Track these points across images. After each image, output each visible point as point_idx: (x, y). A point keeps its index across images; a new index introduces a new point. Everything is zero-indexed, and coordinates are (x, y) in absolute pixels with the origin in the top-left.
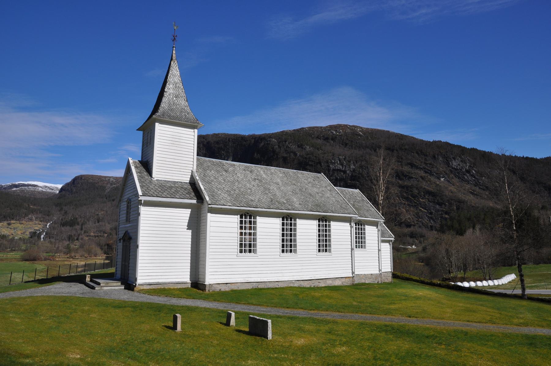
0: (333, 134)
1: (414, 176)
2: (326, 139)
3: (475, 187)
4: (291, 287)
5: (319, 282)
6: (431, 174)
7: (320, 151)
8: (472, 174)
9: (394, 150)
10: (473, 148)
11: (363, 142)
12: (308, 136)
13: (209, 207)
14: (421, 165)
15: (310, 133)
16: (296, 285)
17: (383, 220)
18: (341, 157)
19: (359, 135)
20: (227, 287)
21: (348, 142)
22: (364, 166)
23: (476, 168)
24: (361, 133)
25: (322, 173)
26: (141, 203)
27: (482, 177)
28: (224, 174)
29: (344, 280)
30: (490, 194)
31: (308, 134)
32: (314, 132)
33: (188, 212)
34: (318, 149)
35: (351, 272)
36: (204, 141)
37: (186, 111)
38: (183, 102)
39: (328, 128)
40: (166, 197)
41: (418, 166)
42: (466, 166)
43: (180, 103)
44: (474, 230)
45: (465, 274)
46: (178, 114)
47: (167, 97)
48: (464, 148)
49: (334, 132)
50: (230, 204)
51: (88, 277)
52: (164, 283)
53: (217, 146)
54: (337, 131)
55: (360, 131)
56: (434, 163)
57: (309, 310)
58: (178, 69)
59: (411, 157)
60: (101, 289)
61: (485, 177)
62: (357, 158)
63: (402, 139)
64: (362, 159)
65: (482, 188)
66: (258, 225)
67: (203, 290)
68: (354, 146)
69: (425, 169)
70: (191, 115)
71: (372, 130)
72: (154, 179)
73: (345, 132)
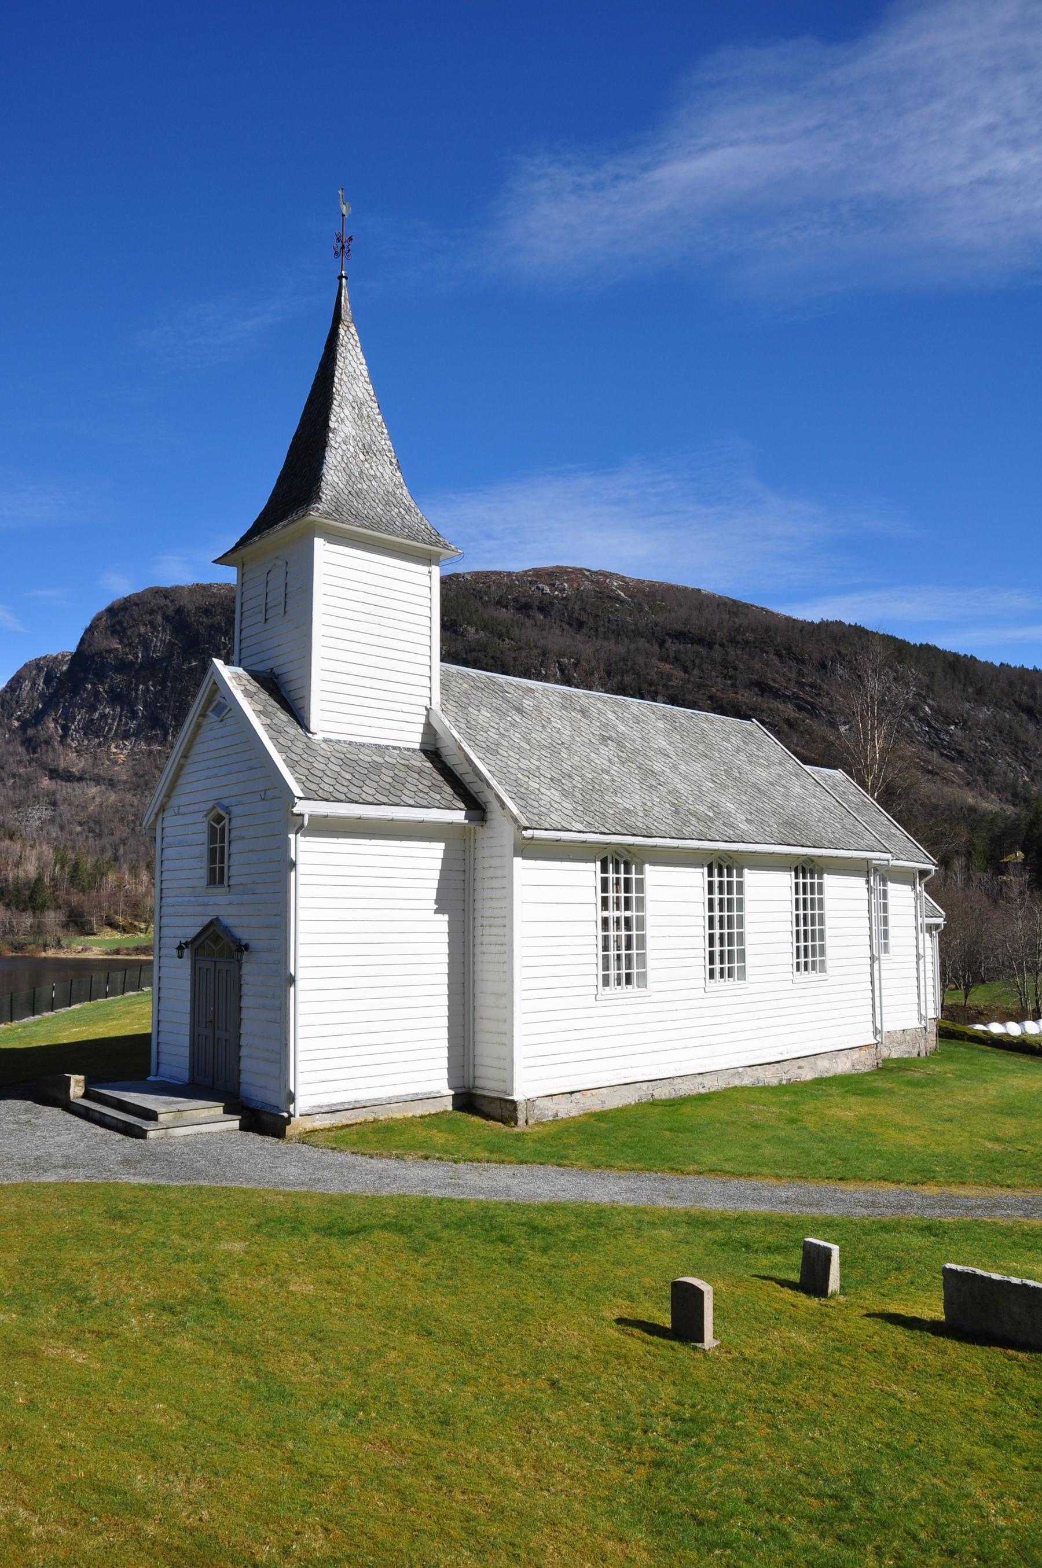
0: (543, 594)
1: (767, 718)
2: (524, 608)
3: (930, 753)
4: (735, 1088)
5: (800, 1068)
6: (813, 711)
7: (507, 641)
8: (922, 714)
9: (715, 644)
10: (927, 645)
11: (628, 619)
12: (472, 597)
13: (524, 838)
14: (786, 688)
15: (478, 589)
16: (747, 1081)
17: (934, 864)
18: (566, 661)
19: (618, 599)
20: (573, 1105)
21: (584, 617)
22: (631, 689)
23: (933, 700)
24: (623, 594)
25: (754, 720)
26: (302, 826)
27: (949, 725)
28: (518, 720)
29: (855, 1055)
30: (967, 770)
31: (471, 591)
32: (489, 587)
33: (435, 851)
34: (500, 637)
35: (872, 1029)
36: (166, 606)
37: (400, 504)
38: (388, 472)
39: (529, 576)
40: (375, 802)
41: (779, 690)
42: (907, 693)
43: (378, 474)
44: (949, 873)
45: (966, 997)
46: (378, 509)
47: (340, 450)
48: (904, 643)
49: (547, 590)
50: (581, 827)
51: (77, 1081)
52: (376, 1103)
53: (205, 620)
54: (553, 585)
55: (620, 588)
56: (822, 684)
57: (908, 1184)
58: (361, 355)
59: (760, 664)
60: (166, 1134)
61: (956, 724)
62: (610, 665)
63: (736, 614)
64: (624, 667)
65: (947, 756)
66: (650, 893)
67: (504, 1120)
68: (601, 629)
69: (797, 698)
70: (417, 514)
71: (653, 585)
72: (315, 737)
73: (578, 589)
